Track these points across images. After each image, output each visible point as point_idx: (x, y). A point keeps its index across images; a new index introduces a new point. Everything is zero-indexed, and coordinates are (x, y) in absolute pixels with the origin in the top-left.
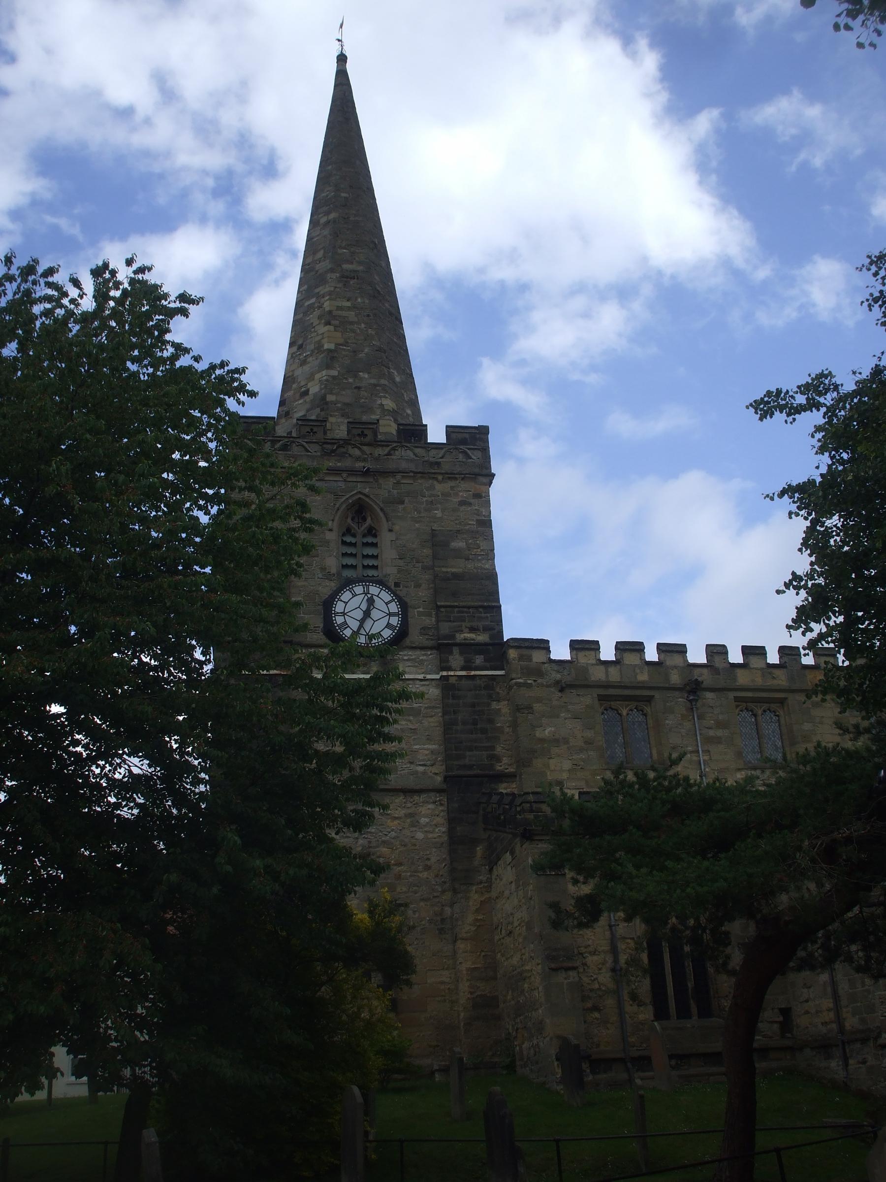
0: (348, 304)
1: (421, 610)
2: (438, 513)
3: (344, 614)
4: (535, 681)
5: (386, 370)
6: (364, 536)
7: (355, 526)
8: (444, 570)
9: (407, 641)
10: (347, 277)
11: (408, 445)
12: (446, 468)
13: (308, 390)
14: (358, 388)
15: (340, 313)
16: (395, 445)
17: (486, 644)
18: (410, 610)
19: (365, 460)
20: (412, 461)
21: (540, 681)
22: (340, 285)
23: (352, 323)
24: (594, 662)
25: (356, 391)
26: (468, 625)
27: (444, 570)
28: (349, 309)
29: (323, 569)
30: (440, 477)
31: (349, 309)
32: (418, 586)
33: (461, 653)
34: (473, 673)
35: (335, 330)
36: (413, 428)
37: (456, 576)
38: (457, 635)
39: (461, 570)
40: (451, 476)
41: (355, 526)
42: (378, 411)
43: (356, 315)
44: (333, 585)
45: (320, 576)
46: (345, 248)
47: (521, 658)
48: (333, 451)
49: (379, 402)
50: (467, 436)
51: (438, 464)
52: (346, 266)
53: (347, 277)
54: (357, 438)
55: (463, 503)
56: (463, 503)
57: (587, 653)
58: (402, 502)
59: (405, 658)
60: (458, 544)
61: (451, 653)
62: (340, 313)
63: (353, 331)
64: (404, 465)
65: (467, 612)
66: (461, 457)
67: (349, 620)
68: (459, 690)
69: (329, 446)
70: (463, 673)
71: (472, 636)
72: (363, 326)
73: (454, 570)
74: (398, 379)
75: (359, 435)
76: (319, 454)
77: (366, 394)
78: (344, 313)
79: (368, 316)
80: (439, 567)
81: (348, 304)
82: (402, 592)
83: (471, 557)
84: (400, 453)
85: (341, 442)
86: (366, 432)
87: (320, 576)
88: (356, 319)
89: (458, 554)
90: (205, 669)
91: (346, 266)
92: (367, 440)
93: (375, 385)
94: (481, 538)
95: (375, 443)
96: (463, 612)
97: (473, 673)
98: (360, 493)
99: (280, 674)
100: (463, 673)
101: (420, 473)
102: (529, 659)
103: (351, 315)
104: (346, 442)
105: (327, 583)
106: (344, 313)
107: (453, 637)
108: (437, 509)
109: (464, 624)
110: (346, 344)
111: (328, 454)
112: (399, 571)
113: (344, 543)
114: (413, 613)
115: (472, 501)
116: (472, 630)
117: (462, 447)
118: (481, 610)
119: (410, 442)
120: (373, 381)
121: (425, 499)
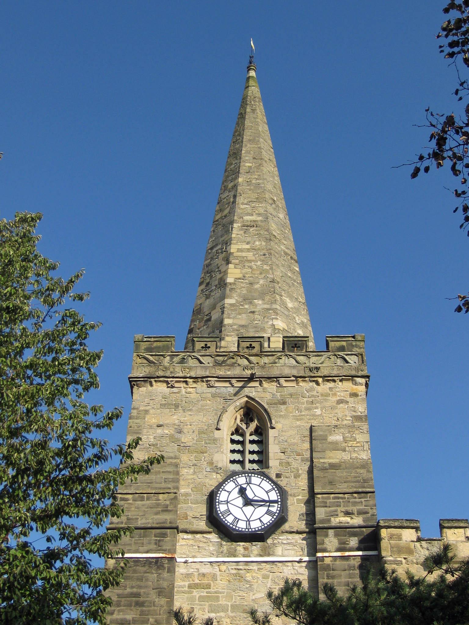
0: (248, 247)
1: (300, 497)
2: (318, 412)
3: (227, 502)
4: (405, 558)
5: (278, 297)
6: (251, 435)
7: (244, 426)
8: (322, 461)
9: (286, 526)
10: (248, 226)
11: (291, 354)
12: (325, 371)
13: (211, 317)
14: (253, 312)
15: (240, 254)
16: (279, 354)
17: (360, 527)
18: (290, 498)
19: (252, 368)
20: (294, 367)
21: (410, 558)
22: (242, 232)
23: (250, 261)
24: (463, 539)
25: (251, 315)
26: (343, 509)
27: (322, 461)
28: (248, 250)
29: (211, 463)
30: (320, 380)
31: (248, 250)
32: (297, 476)
33: (336, 535)
34: (347, 554)
35: (235, 268)
36: (296, 339)
37: (333, 466)
38: (332, 519)
39: (337, 460)
40: (327, 378)
41: (244, 426)
42: (270, 331)
43: (254, 255)
44: (220, 478)
45: (208, 470)
46: (246, 204)
47: (391, 537)
48: (224, 362)
49: (270, 323)
50: (344, 343)
51: (318, 369)
52: (247, 218)
53: (248, 226)
54: (246, 350)
55: (340, 402)
56: (340, 402)
57: (456, 531)
58: (284, 403)
59: (285, 542)
60: (337, 437)
61: (327, 536)
62: (240, 254)
63: (251, 267)
64: (287, 371)
65: (342, 498)
66: (339, 362)
67: (231, 508)
68: (333, 570)
69: (221, 358)
70: (339, 554)
71: (348, 519)
72: (259, 263)
73: (331, 461)
74: (290, 305)
75: (247, 347)
76: (211, 365)
77: (259, 317)
78: (244, 254)
79: (264, 255)
80: (318, 458)
81: (248, 247)
82: (282, 482)
83: (347, 449)
84: (284, 360)
85: (232, 354)
86: (254, 344)
87: (208, 470)
88: (253, 258)
89: (335, 446)
90: (456, 610)
91: (247, 218)
92: (255, 351)
93: (269, 309)
94: (357, 432)
95: (262, 353)
96: (338, 498)
97: (347, 554)
98: (247, 397)
99: (166, 557)
100: (339, 554)
101: (301, 377)
102: (399, 538)
103: (250, 255)
104: (236, 354)
105: (214, 475)
106: (244, 254)
107: (329, 521)
108: (316, 408)
109: (339, 509)
110: (244, 278)
111: (218, 364)
112: (281, 464)
113: (233, 441)
114: (291, 501)
115: (349, 399)
116: (347, 513)
117: (340, 353)
118: (355, 495)
119: (293, 352)
120: (266, 306)
121: (305, 399)
